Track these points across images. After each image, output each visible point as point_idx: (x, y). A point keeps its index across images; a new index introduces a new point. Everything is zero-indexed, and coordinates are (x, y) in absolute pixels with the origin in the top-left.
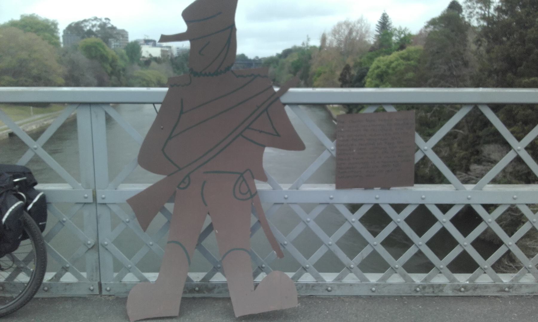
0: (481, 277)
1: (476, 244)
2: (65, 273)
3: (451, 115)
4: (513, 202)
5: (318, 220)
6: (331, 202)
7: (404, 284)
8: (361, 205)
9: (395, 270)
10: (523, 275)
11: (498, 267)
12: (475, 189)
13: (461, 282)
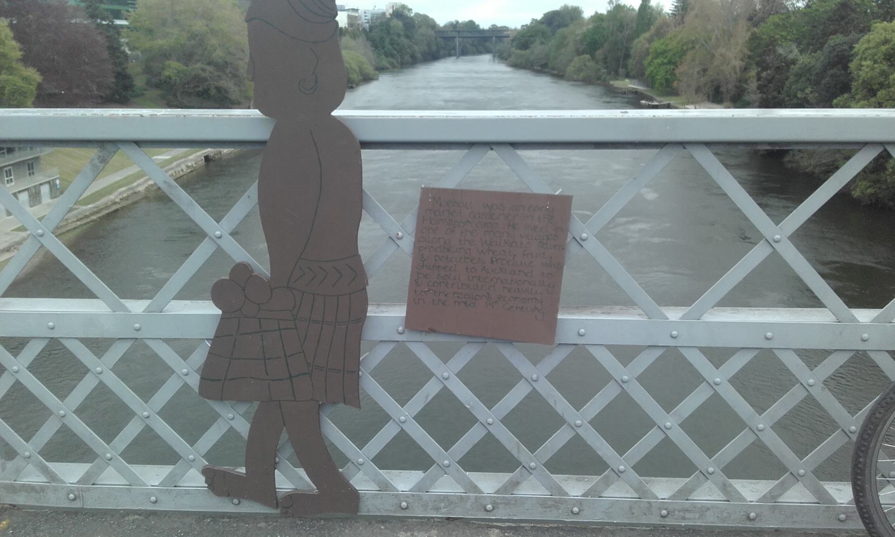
0: (524, 484)
1: (689, 425)
2: (794, 484)
3: (831, 169)
4: (862, 347)
5: (738, 381)
6: (138, 335)
7: (376, 495)
8: (827, 353)
9: (444, 469)
10: (607, 483)
11: (557, 464)
12: (148, 310)
13: (839, 501)
